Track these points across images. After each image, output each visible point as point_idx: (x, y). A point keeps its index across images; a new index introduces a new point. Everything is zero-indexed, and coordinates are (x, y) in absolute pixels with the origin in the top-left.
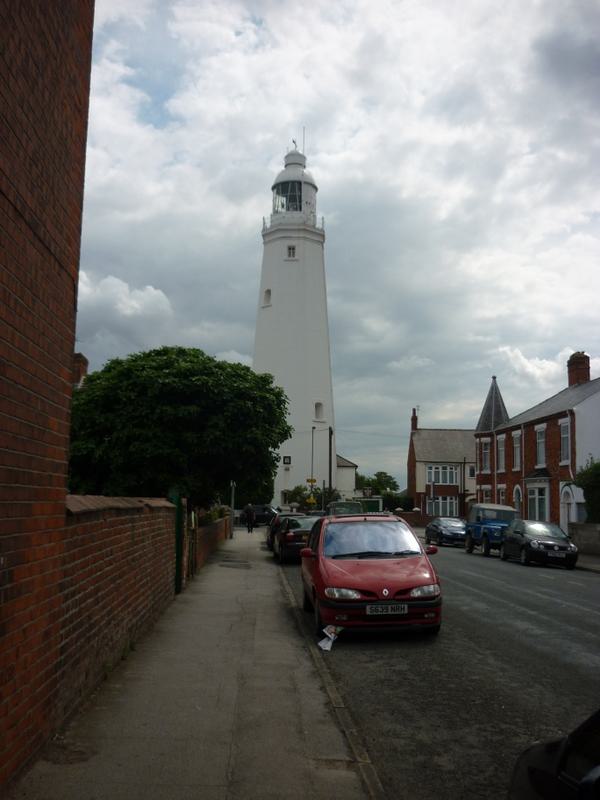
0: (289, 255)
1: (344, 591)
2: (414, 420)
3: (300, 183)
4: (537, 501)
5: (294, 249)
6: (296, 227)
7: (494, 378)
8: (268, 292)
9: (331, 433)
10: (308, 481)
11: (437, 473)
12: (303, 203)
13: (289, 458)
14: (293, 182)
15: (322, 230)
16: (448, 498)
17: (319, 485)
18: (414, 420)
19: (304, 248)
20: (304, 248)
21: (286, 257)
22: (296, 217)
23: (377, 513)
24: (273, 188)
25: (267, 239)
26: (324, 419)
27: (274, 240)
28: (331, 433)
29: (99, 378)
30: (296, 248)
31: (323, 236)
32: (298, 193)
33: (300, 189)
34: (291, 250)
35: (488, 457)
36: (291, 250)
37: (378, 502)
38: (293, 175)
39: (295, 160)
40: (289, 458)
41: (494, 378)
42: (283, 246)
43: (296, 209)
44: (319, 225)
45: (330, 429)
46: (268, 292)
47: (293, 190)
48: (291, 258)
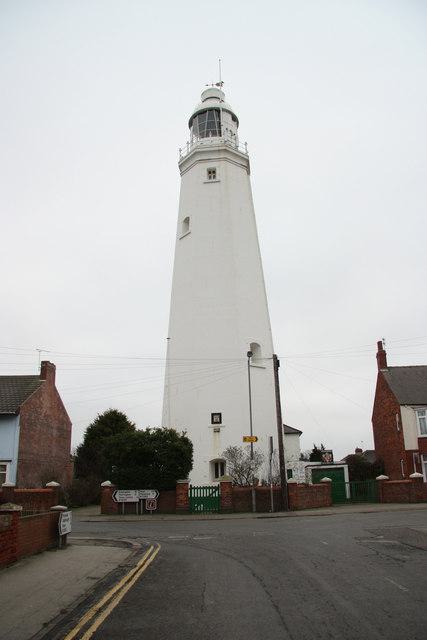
0: (210, 178)
2: (382, 356)
5: (214, 172)
6: (217, 148)
8: (187, 221)
10: (245, 439)
12: (223, 129)
13: (213, 415)
15: (246, 155)
18: (382, 356)
19: (224, 169)
20: (224, 169)
21: (206, 179)
22: (213, 141)
23: (270, 515)
25: (184, 169)
27: (190, 168)
28: (277, 364)
30: (217, 172)
31: (248, 161)
32: (216, 120)
33: (219, 116)
34: (212, 173)
36: (212, 173)
37: (342, 469)
40: (220, 414)
42: (201, 170)
43: (214, 134)
44: (241, 149)
45: (275, 357)
46: (187, 221)
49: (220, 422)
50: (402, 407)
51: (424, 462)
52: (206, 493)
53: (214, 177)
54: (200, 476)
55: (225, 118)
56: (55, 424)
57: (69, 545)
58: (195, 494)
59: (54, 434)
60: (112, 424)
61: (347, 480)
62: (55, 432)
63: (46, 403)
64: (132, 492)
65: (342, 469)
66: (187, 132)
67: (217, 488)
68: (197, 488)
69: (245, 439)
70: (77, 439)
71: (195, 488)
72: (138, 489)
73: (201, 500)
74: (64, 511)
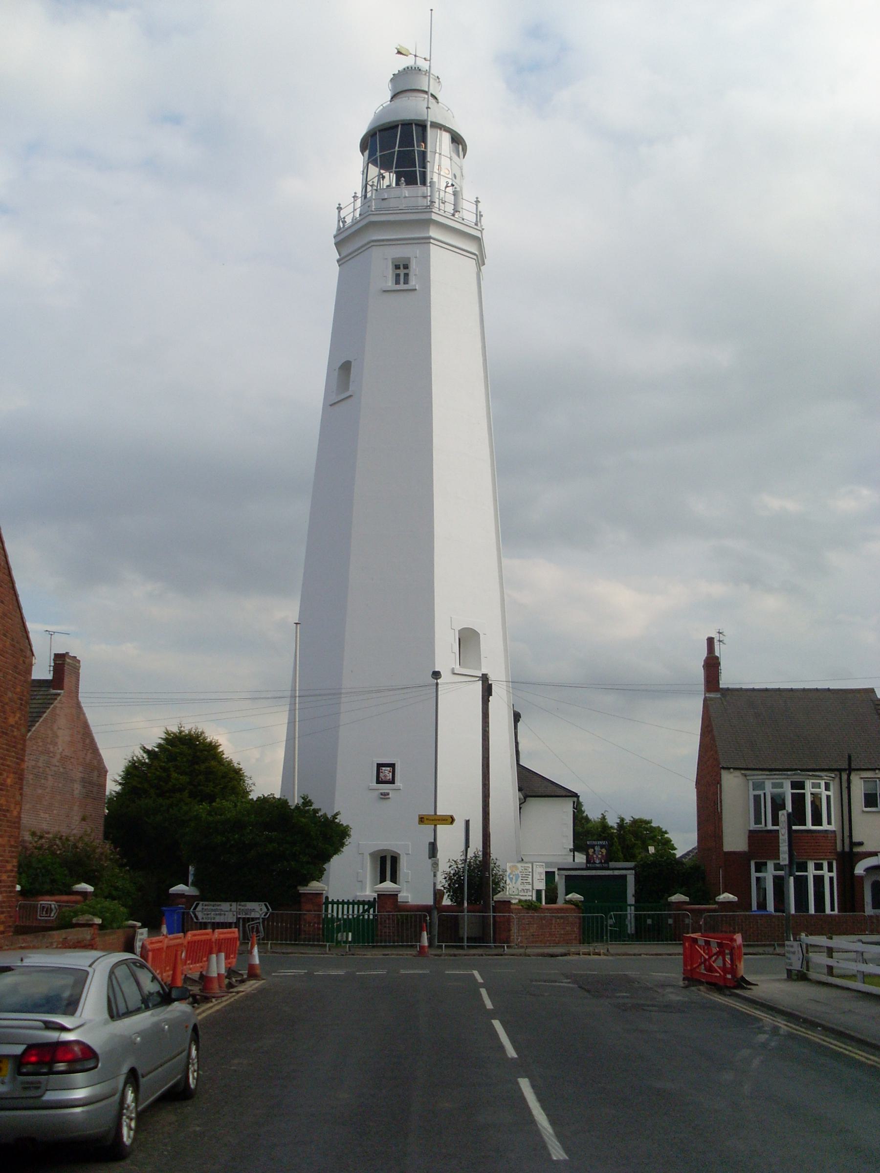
0: (397, 282)
2: (712, 665)
3: (422, 126)
5: (406, 267)
8: (346, 368)
18: (712, 665)
21: (390, 284)
25: (348, 249)
37: (624, 877)
40: (392, 766)
45: (485, 678)
46: (346, 368)
49: (392, 782)
50: (723, 772)
51: (131, 922)
52: (352, 912)
53: (406, 282)
54: (346, 880)
55: (439, 146)
56: (77, 773)
57: (303, 798)
58: (333, 912)
59: (76, 792)
60: (187, 766)
61: (631, 900)
62: (77, 788)
63: (63, 737)
64: (225, 906)
65: (624, 877)
66: (358, 159)
67: (371, 904)
68: (338, 903)
69: (422, 820)
70: (112, 787)
71: (333, 903)
72: (236, 901)
73: (348, 924)
74: (140, 928)
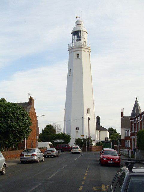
1: (54, 141)
2: (122, 113)
3: (80, 31)
4: (127, 135)
5: (79, 55)
6: (79, 47)
7: (136, 98)
9: (89, 119)
11: (128, 132)
14: (78, 31)
16: (127, 141)
17: (85, 137)
18: (122, 113)
21: (76, 58)
24: (72, 33)
26: (91, 114)
28: (89, 119)
29: (11, 107)
30: (80, 55)
35: (134, 126)
38: (78, 29)
39: (78, 24)
41: (136, 98)
47: (78, 34)
48: (78, 58)
